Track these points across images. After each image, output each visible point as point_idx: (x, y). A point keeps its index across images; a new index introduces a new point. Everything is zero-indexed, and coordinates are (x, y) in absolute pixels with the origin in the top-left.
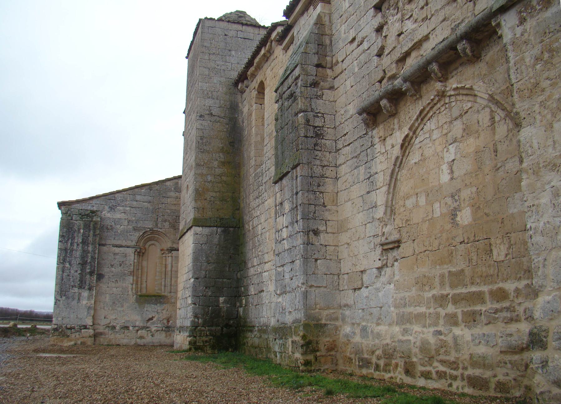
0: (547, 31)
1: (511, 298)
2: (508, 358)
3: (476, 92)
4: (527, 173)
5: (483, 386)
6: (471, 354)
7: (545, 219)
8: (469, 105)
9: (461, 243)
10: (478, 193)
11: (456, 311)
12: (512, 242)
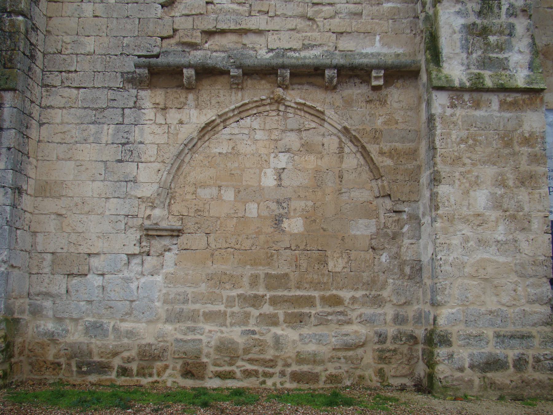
0: (474, 125)
1: (346, 304)
2: (341, 354)
3: (326, 118)
4: (442, 219)
5: (311, 380)
6: (298, 352)
7: (455, 255)
8: (313, 125)
9: (285, 249)
10: (315, 208)
11: (276, 311)
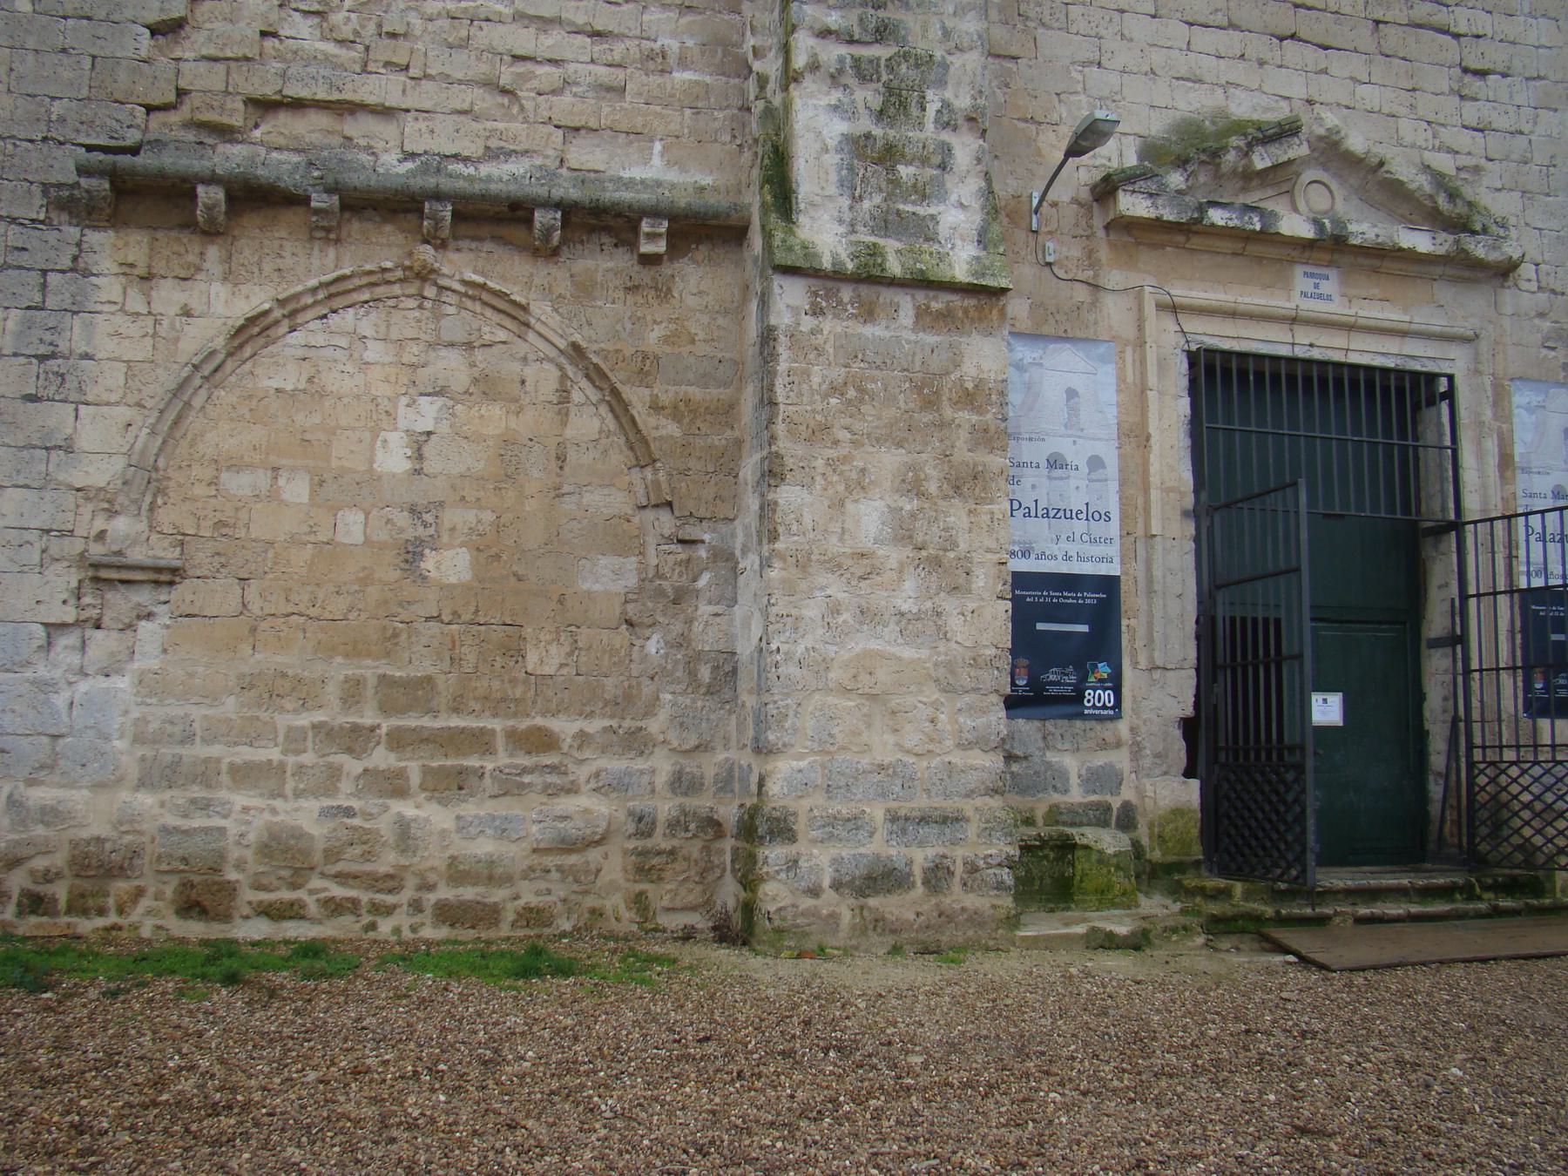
2: (550, 861)
3: (533, 321)
4: (785, 561)
7: (808, 642)
8: (502, 335)
9: (428, 619)
10: (498, 527)
11: (403, 764)
12: (580, 644)
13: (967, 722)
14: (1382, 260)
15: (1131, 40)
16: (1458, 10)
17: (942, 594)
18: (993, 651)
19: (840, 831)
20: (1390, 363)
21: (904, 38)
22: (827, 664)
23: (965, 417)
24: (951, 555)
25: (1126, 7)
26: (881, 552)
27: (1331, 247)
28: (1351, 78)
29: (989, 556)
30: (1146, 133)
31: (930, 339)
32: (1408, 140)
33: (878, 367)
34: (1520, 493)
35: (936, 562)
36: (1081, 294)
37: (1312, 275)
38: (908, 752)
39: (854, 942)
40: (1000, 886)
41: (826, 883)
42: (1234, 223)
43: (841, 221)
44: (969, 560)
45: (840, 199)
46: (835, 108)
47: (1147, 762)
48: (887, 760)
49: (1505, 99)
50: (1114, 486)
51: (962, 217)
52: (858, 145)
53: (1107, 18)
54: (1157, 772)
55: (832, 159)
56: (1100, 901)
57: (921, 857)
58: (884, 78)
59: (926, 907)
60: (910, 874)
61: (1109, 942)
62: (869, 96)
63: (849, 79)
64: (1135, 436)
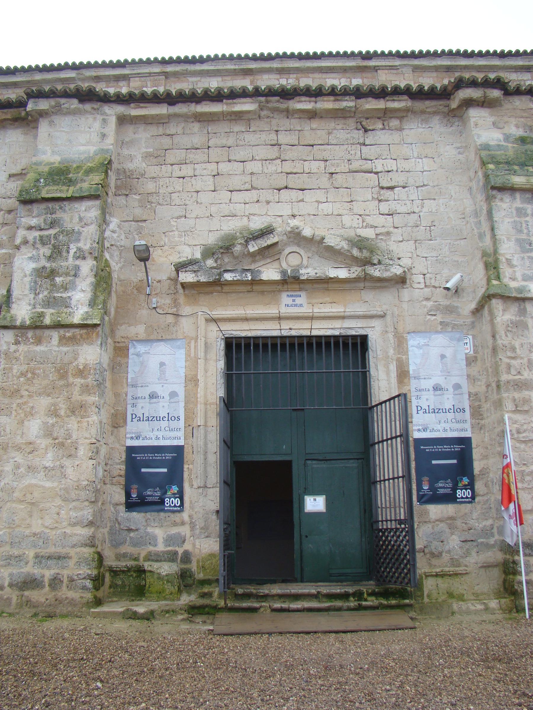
13: (73, 514)
14: (323, 284)
15: (201, 203)
16: (376, 161)
17: (64, 458)
18: (86, 483)
19: (13, 562)
20: (337, 333)
21: (62, 224)
22: (13, 490)
23: (79, 381)
24: (69, 441)
25: (200, 190)
26: (38, 442)
27: (291, 282)
28: (316, 201)
29: (86, 440)
30: (206, 243)
31: (65, 349)
32: (348, 225)
33: (42, 363)
34: (413, 389)
35: (62, 445)
36: (170, 319)
37: (292, 296)
38: (47, 527)
39: (17, 611)
40: (84, 588)
41: (6, 584)
42: (239, 278)
43: (30, 304)
44: (77, 443)
45: (30, 295)
46: (31, 258)
47: (197, 532)
48: (38, 531)
49: (405, 198)
50: (182, 404)
51: (83, 295)
52: (39, 273)
53: (190, 196)
54: (203, 536)
55: (28, 279)
56: (158, 597)
57: (48, 574)
58: (53, 242)
59: (50, 596)
60: (43, 581)
61: (135, 616)
62: (46, 251)
63: (39, 246)
64: (192, 381)
